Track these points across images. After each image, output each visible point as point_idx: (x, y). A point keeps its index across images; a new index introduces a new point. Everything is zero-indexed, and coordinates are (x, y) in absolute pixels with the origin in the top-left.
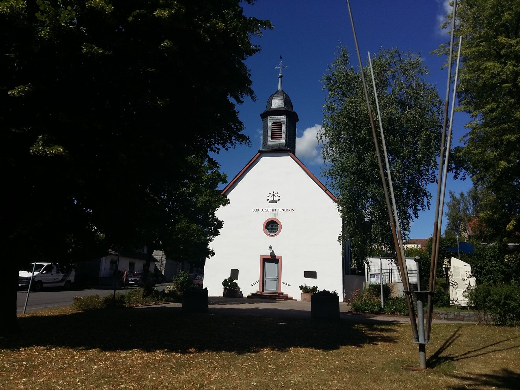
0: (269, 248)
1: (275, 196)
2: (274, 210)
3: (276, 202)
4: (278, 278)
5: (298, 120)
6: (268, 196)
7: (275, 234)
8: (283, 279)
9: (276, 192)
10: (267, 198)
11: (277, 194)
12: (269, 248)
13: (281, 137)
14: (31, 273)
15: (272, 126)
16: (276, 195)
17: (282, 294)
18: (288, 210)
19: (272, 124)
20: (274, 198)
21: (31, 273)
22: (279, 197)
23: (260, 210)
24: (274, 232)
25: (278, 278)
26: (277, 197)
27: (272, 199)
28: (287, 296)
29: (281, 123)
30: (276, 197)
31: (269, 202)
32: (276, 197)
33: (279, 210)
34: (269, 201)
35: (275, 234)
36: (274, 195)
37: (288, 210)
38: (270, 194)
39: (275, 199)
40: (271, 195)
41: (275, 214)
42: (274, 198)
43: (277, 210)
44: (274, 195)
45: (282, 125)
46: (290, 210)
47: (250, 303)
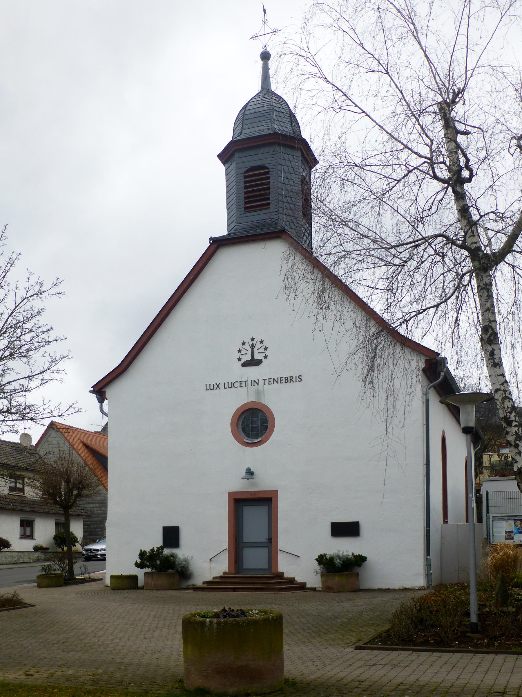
0: (244, 474)
1: (255, 349)
2: (255, 382)
3: (258, 362)
4: (270, 540)
5: (294, 578)
6: (240, 351)
7: (260, 439)
8: (283, 543)
9: (258, 338)
10: (238, 355)
11: (261, 342)
12: (245, 474)
13: (269, 204)
14: (486, 282)
15: (245, 177)
16: (258, 345)
17: (281, 575)
18: (288, 380)
19: (245, 172)
20: (253, 354)
21: (486, 282)
22: (266, 349)
23: (221, 386)
24: (257, 436)
25: (270, 540)
26: (262, 350)
27: (248, 357)
28: (292, 580)
29: (267, 168)
30: (259, 351)
31: (244, 365)
32: (259, 351)
33: (267, 382)
34: (243, 361)
35: (260, 439)
36: (253, 347)
37: (288, 380)
38: (244, 344)
39: (257, 357)
40: (247, 347)
41: (258, 393)
42: (253, 354)
43: (261, 382)
44: (253, 347)
45: (268, 173)
46: (294, 380)
47: (274, 426)
